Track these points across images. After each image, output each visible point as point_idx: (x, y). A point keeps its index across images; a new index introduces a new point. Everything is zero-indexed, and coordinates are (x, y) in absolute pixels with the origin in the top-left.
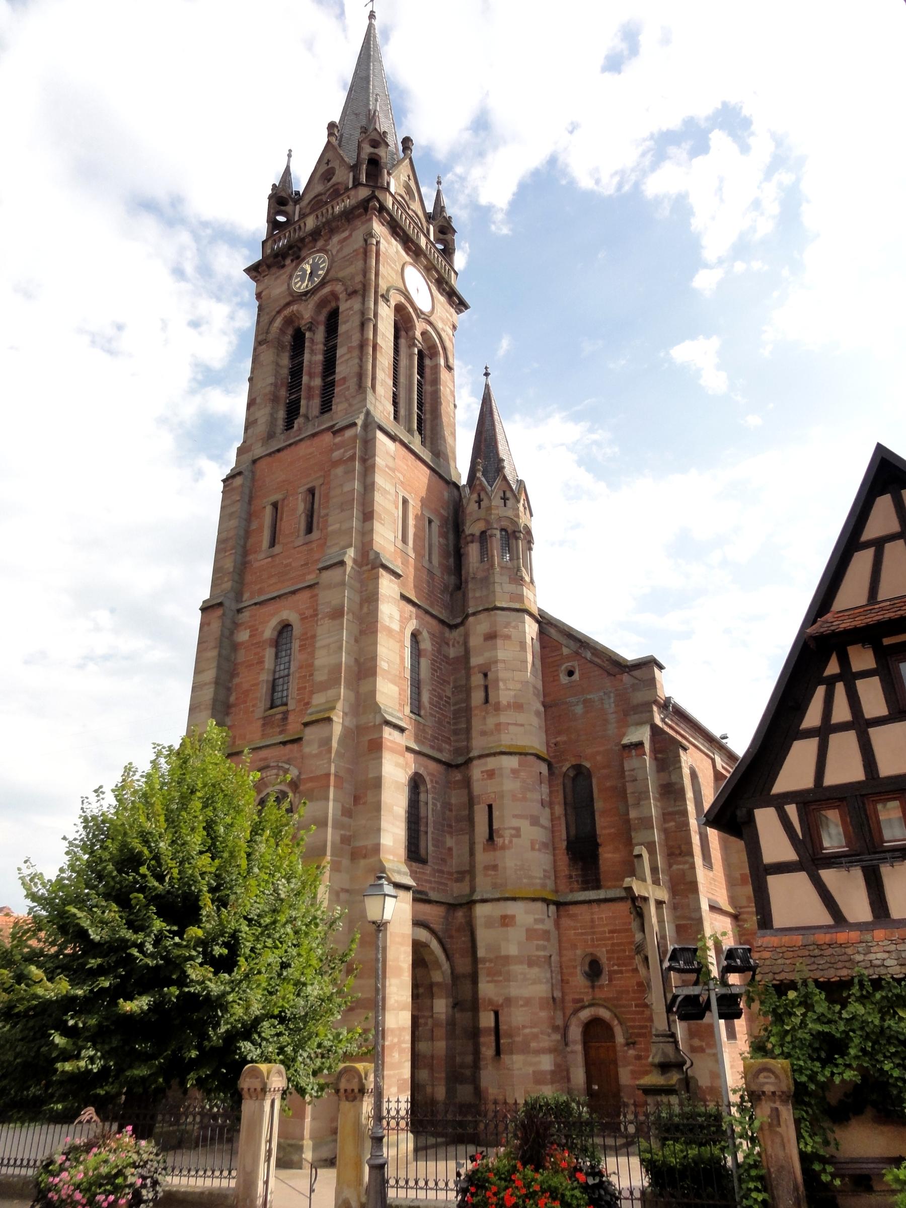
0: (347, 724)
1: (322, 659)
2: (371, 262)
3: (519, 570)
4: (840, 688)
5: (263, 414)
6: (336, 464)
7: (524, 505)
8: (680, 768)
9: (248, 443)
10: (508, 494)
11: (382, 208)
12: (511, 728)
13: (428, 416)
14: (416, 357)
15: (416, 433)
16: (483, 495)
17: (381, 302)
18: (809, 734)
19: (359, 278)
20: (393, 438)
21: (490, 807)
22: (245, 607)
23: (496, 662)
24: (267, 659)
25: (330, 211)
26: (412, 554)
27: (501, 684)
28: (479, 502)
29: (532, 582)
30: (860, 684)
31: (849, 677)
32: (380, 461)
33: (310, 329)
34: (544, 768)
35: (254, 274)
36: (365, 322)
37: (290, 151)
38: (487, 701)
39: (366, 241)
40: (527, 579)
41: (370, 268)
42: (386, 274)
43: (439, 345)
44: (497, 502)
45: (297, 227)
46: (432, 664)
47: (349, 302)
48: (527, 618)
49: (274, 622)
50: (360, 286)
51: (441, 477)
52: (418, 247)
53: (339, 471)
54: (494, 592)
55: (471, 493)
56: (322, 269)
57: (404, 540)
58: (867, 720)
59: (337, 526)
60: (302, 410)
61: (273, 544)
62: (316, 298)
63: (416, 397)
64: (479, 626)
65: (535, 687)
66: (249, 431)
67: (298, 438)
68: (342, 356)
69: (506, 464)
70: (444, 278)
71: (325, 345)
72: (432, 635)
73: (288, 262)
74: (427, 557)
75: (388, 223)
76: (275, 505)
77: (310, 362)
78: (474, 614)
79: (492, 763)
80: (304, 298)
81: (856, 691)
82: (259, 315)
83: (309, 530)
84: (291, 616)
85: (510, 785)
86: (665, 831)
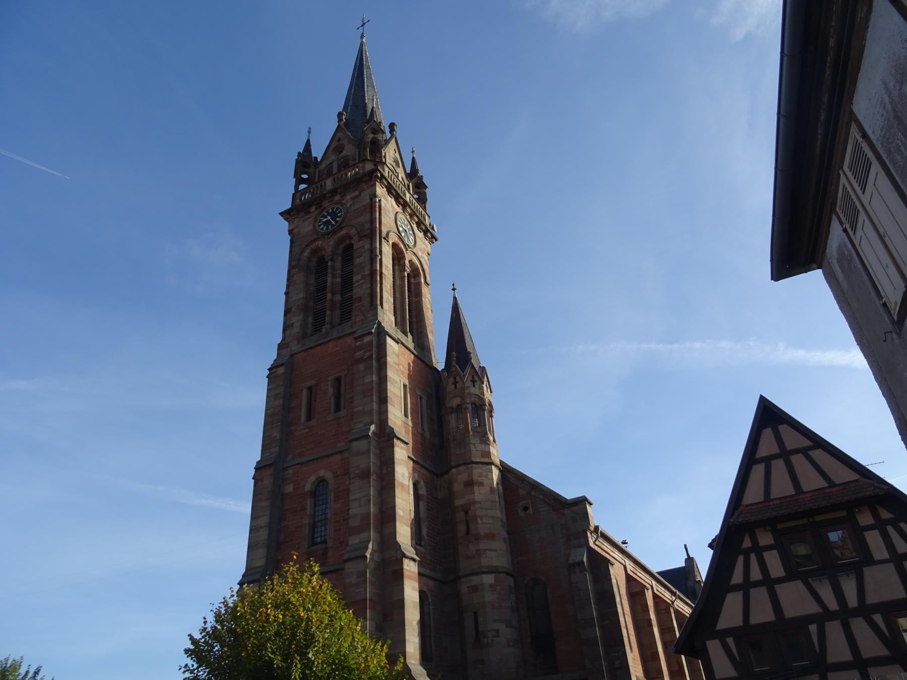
0: (376, 559)
1: (355, 510)
2: (376, 214)
3: (486, 434)
4: (753, 557)
5: (297, 321)
6: (360, 361)
7: (486, 386)
8: (611, 579)
9: (287, 340)
10: (476, 378)
11: (383, 177)
12: (488, 552)
13: (414, 320)
14: (406, 279)
15: (409, 334)
16: (458, 379)
17: (384, 242)
18: (736, 588)
19: (367, 226)
20: (397, 341)
21: (476, 614)
22: (289, 467)
23: (474, 503)
24: (308, 507)
25: (344, 176)
26: (410, 424)
27: (479, 520)
28: (455, 383)
29: (494, 441)
30: (766, 555)
31: (759, 550)
32: (390, 359)
33: (332, 260)
34: (511, 581)
35: (287, 216)
36: (373, 257)
37: (310, 128)
38: (468, 533)
39: (371, 199)
40: (491, 439)
41: (376, 219)
42: (386, 223)
43: (420, 268)
44: (469, 384)
45: (319, 186)
46: (427, 505)
47: (361, 242)
48: (493, 467)
49: (313, 479)
50: (368, 232)
51: (426, 364)
52: (405, 201)
53: (361, 367)
54: (470, 451)
55: (449, 377)
56: (340, 217)
57: (406, 415)
58: (773, 580)
59: (360, 408)
60: (328, 319)
61: (309, 418)
62: (336, 237)
63: (407, 308)
64: (460, 476)
65: (501, 520)
66: (287, 332)
67: (325, 340)
68: (358, 281)
69: (472, 355)
70: (421, 221)
71: (342, 271)
72: (426, 483)
73: (313, 209)
74: (420, 425)
75: (386, 187)
76: (310, 389)
77: (332, 283)
78: (456, 467)
79: (475, 580)
80: (326, 237)
81: (764, 559)
82: (291, 246)
83: (338, 409)
84: (328, 475)
85: (490, 597)
86: (602, 628)
